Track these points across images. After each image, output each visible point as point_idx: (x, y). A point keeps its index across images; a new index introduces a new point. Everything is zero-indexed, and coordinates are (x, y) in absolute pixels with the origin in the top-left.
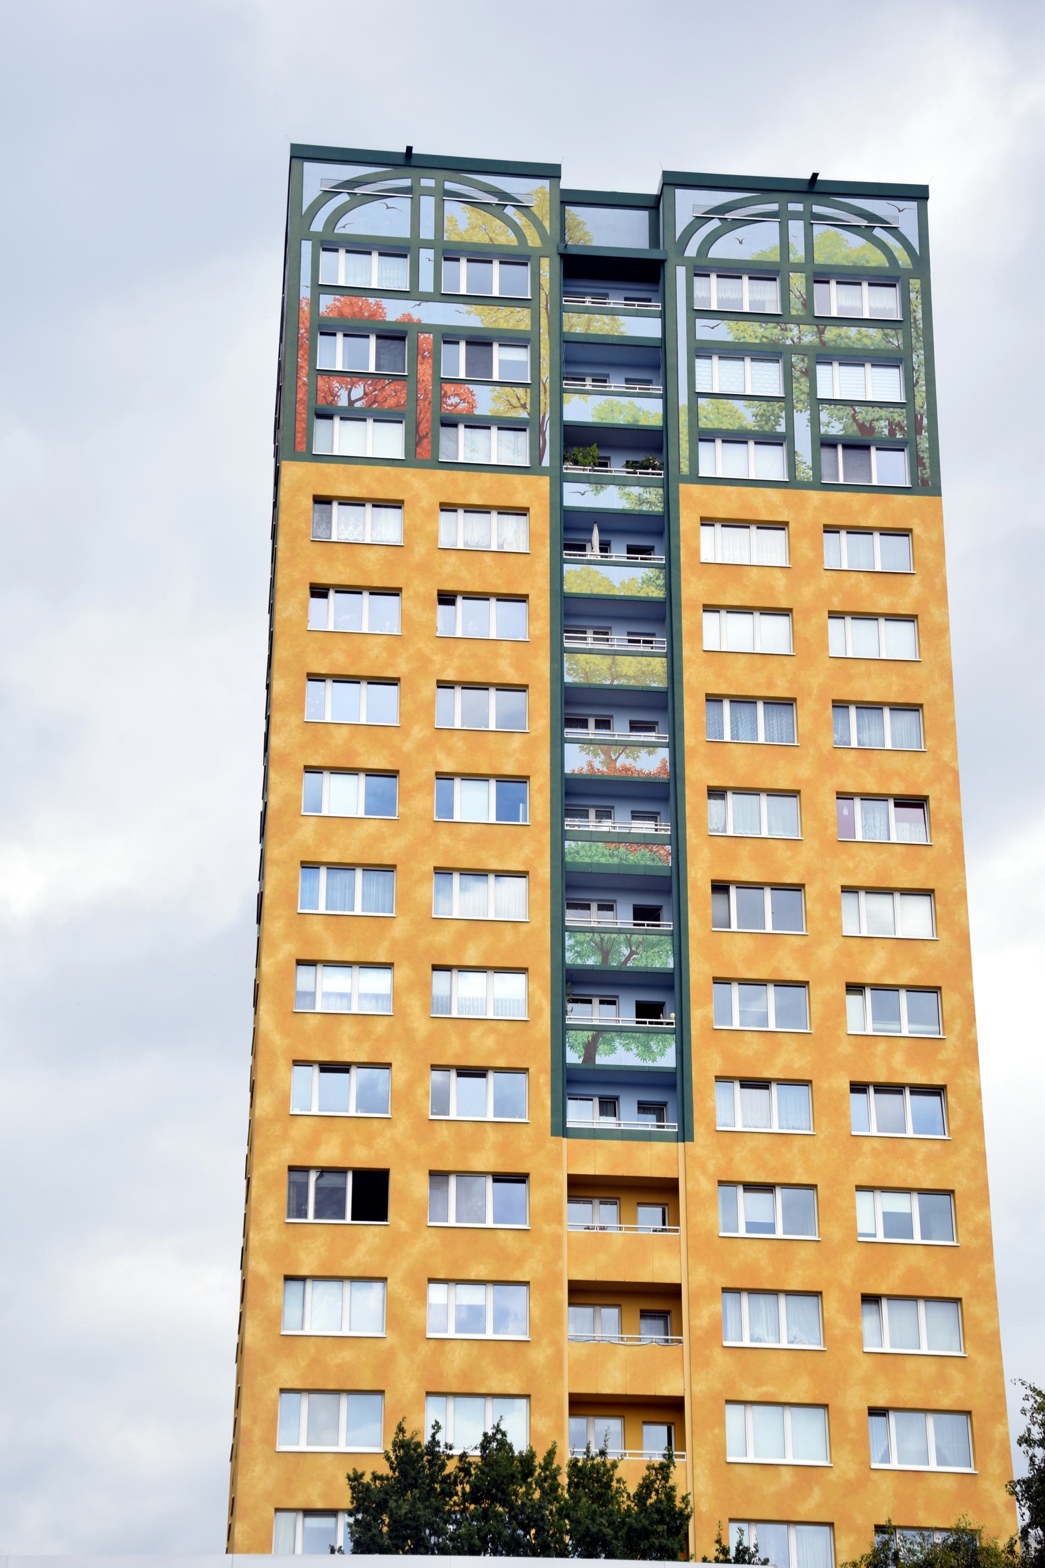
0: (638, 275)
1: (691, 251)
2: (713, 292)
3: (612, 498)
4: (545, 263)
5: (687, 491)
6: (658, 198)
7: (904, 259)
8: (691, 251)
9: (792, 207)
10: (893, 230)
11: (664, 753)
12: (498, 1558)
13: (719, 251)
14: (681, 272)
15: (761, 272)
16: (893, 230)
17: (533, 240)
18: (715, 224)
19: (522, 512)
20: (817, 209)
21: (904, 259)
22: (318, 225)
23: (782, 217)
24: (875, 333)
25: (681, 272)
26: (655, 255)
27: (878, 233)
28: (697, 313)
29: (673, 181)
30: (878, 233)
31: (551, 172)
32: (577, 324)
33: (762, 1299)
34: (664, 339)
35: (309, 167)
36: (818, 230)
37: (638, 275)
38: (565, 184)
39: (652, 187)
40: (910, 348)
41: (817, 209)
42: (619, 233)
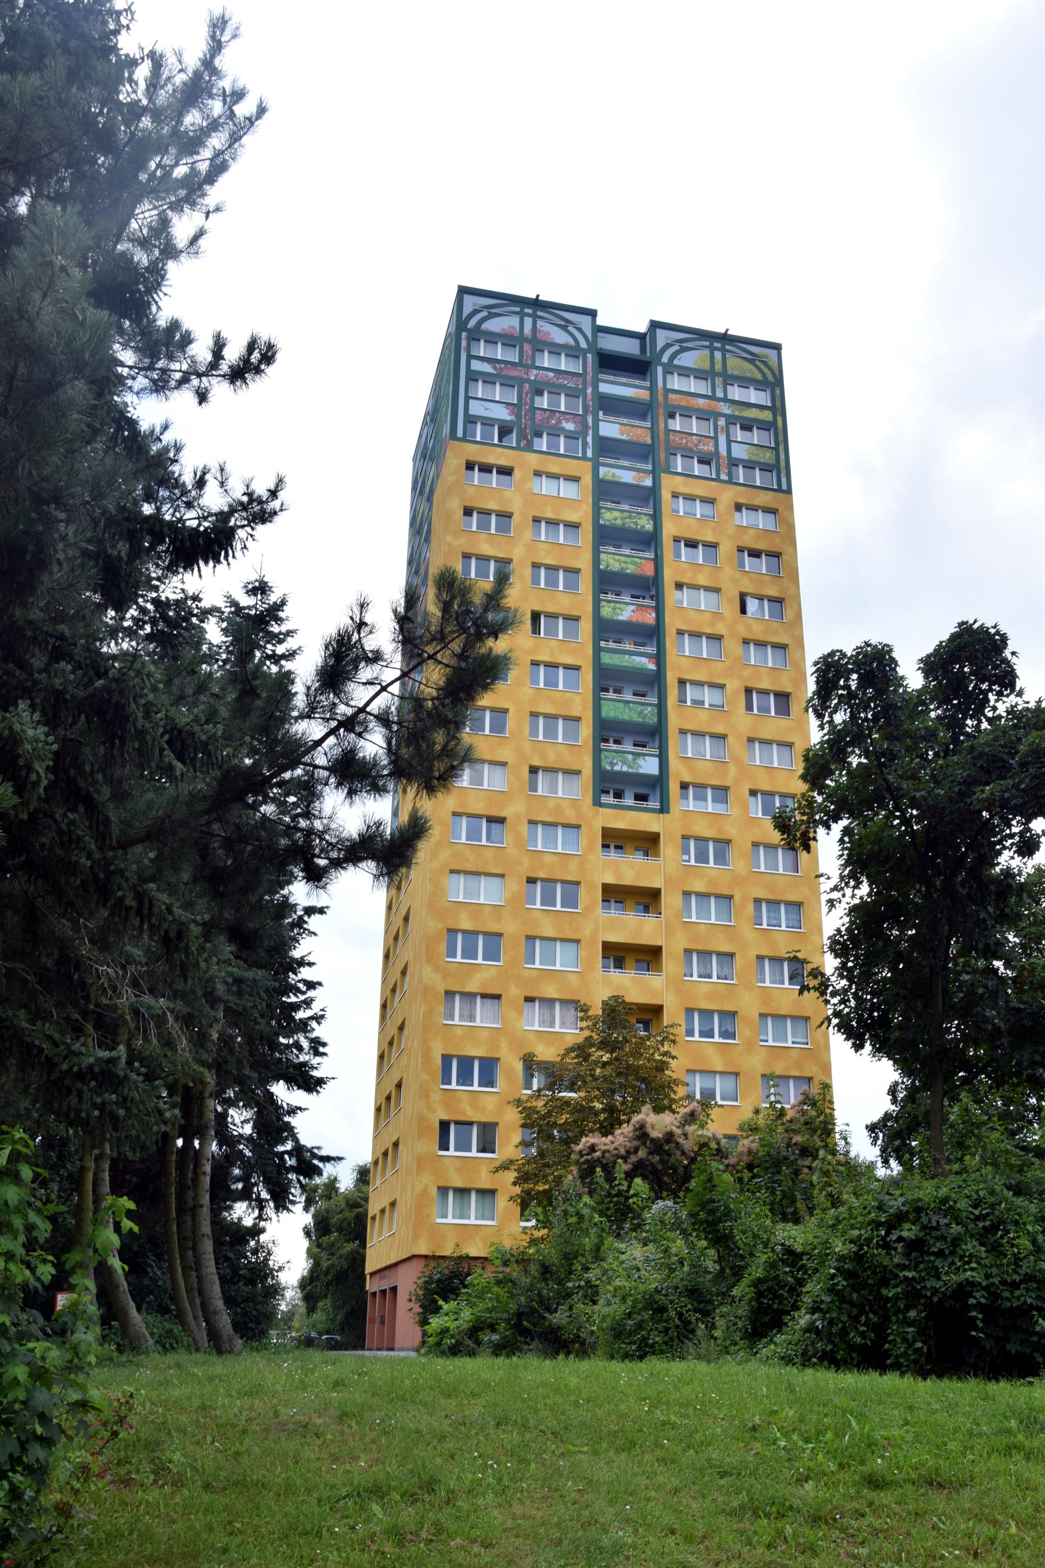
0: (636, 367)
1: (665, 359)
2: (676, 383)
3: (627, 477)
4: (589, 356)
5: (665, 478)
6: (645, 335)
7: (771, 378)
8: (665, 359)
9: (527, 310)
10: (580, 330)
11: (654, 615)
12: (835, 1100)
13: (488, 326)
14: (660, 369)
15: (700, 375)
16: (580, 330)
17: (583, 345)
18: (676, 348)
19: (576, 479)
20: (539, 313)
21: (771, 378)
22: (472, 324)
23: (522, 315)
24: (551, 375)
25: (660, 369)
26: (643, 358)
27: (571, 328)
28: (668, 391)
29: (655, 325)
30: (571, 328)
31: (592, 313)
32: (604, 388)
33: (489, 1001)
34: (651, 400)
35: (658, 331)
36: (539, 323)
37: (636, 367)
38: (600, 321)
39: (642, 328)
40: (585, 388)
41: (539, 313)
42: (630, 348)
